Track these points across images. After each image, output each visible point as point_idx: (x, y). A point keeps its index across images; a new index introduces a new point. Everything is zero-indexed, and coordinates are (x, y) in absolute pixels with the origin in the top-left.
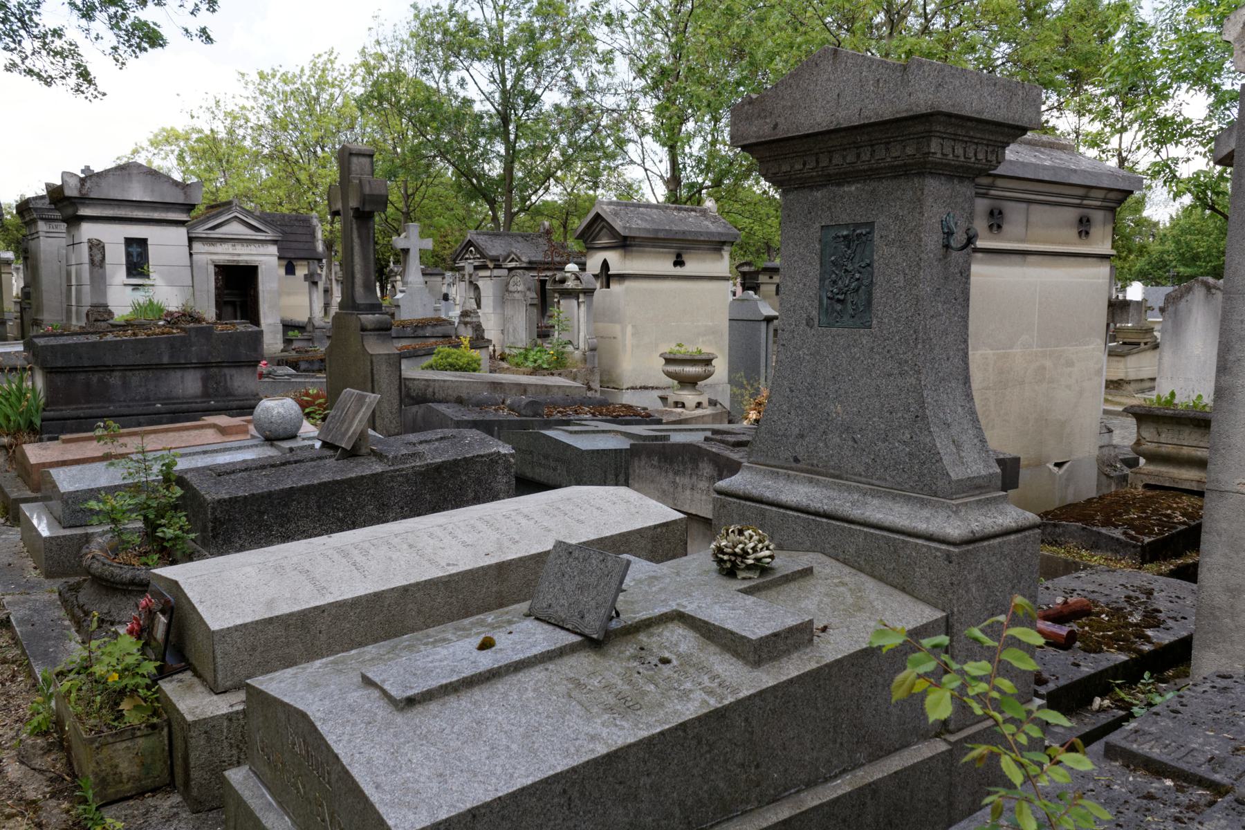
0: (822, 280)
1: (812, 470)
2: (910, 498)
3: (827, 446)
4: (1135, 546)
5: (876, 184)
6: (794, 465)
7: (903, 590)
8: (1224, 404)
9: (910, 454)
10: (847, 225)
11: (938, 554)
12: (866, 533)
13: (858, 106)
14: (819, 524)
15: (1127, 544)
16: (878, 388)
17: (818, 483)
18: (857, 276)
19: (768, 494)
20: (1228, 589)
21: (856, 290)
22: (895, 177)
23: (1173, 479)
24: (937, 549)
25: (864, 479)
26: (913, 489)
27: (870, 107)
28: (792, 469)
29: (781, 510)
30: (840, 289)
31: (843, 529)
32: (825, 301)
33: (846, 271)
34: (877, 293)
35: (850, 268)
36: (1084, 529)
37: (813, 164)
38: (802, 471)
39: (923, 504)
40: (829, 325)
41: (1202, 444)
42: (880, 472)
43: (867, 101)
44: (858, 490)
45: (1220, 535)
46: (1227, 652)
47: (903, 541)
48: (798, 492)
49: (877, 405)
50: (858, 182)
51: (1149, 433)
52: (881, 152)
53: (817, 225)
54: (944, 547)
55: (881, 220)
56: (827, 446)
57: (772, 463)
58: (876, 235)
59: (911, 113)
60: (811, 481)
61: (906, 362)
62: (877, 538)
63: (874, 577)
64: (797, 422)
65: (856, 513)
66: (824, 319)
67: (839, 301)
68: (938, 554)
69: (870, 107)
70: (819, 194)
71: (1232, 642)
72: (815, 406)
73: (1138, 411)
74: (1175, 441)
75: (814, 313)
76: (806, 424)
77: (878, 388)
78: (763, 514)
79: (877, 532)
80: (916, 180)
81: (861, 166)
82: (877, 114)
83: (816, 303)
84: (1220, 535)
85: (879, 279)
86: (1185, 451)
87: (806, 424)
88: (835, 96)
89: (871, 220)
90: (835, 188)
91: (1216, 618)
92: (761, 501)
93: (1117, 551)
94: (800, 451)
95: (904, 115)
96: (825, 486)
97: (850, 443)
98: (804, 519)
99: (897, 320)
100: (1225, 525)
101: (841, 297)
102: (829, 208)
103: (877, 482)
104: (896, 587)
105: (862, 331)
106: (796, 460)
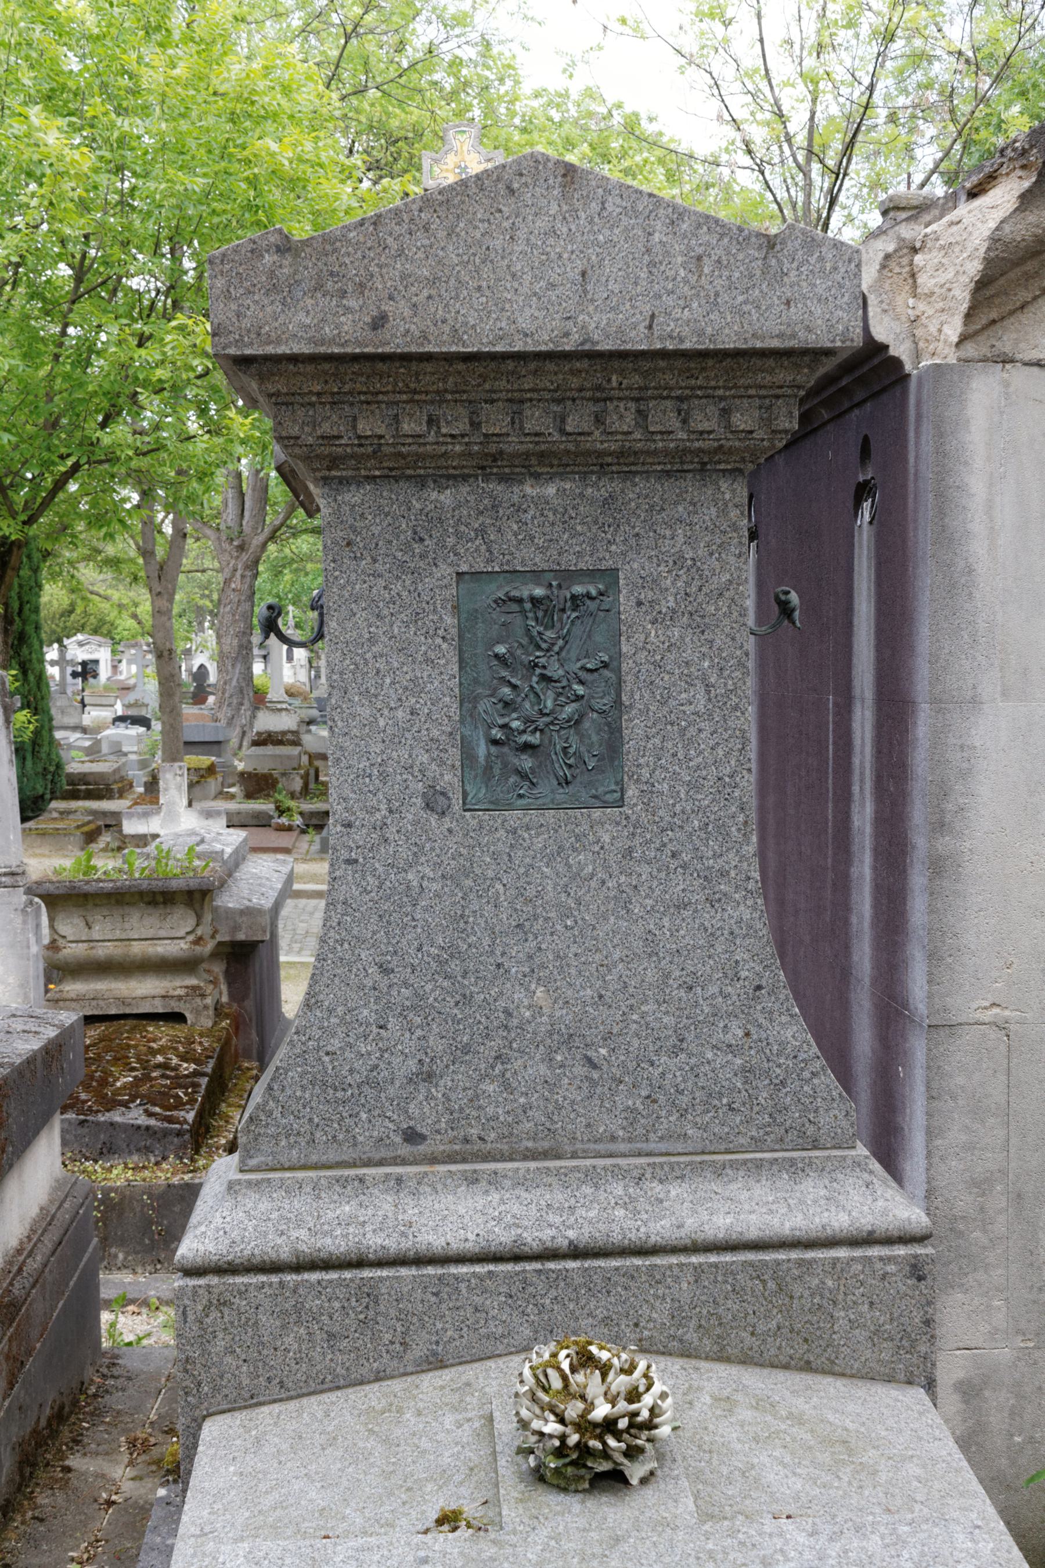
0: (467, 700)
1: (471, 1153)
2: (759, 1165)
3: (507, 1086)
4: (179, 1134)
5: (616, 485)
6: (405, 1150)
7: (808, 1367)
8: (945, 883)
9: (746, 1071)
10: (536, 575)
11: (891, 1268)
12: (698, 1269)
13: (647, 310)
14: (564, 1276)
15: (166, 1133)
16: (649, 938)
17: (495, 1180)
18: (580, 690)
19: (375, 1241)
20: (975, 1183)
21: (576, 722)
22: (668, 473)
23: (123, 1001)
24: (890, 1259)
25: (623, 1147)
26: (758, 1144)
27: (677, 313)
28: (404, 1162)
29: (430, 1270)
30: (528, 721)
31: (631, 1275)
32: (482, 750)
33: (545, 678)
34: (634, 729)
35: (555, 670)
36: (82, 1123)
37: (462, 426)
38: (433, 1160)
39: (796, 1170)
40: (496, 805)
41: (162, 933)
42: (669, 1121)
43: (669, 301)
44: (617, 1173)
45: (954, 1098)
46: (980, 1285)
47: (800, 1263)
48: (456, 1214)
49: (651, 976)
50: (562, 476)
51: (70, 927)
52: (664, 417)
53: (445, 570)
54: (901, 1251)
55: (633, 568)
56: (507, 1086)
57: (332, 1156)
58: (625, 601)
59: (793, 343)
60: (472, 1180)
61: (723, 874)
62: (728, 1271)
63: (728, 1360)
64: (409, 1043)
65: (659, 1229)
66: (478, 792)
67: (527, 747)
68: (891, 1268)
69: (677, 313)
70: (447, 497)
71: (987, 1267)
72: (467, 999)
73: (51, 888)
74: (118, 934)
75: (449, 779)
76: (438, 1045)
77: (649, 938)
78: (370, 1294)
79: (728, 1257)
80: (724, 485)
81: (597, 441)
82: (701, 333)
83: (454, 755)
84: (954, 1098)
85: (634, 694)
86: (137, 949)
87: (438, 1045)
88: (574, 275)
89: (609, 564)
90: (497, 488)
91: (960, 1234)
92: (360, 1263)
93: (148, 1150)
94: (424, 1112)
95: (775, 343)
96: (521, 1183)
97: (580, 1070)
98: (509, 1276)
99: (694, 786)
100: (960, 1080)
101: (535, 739)
102: (481, 532)
103: (663, 1147)
104: (786, 1367)
105: (597, 814)
106: (412, 1136)
